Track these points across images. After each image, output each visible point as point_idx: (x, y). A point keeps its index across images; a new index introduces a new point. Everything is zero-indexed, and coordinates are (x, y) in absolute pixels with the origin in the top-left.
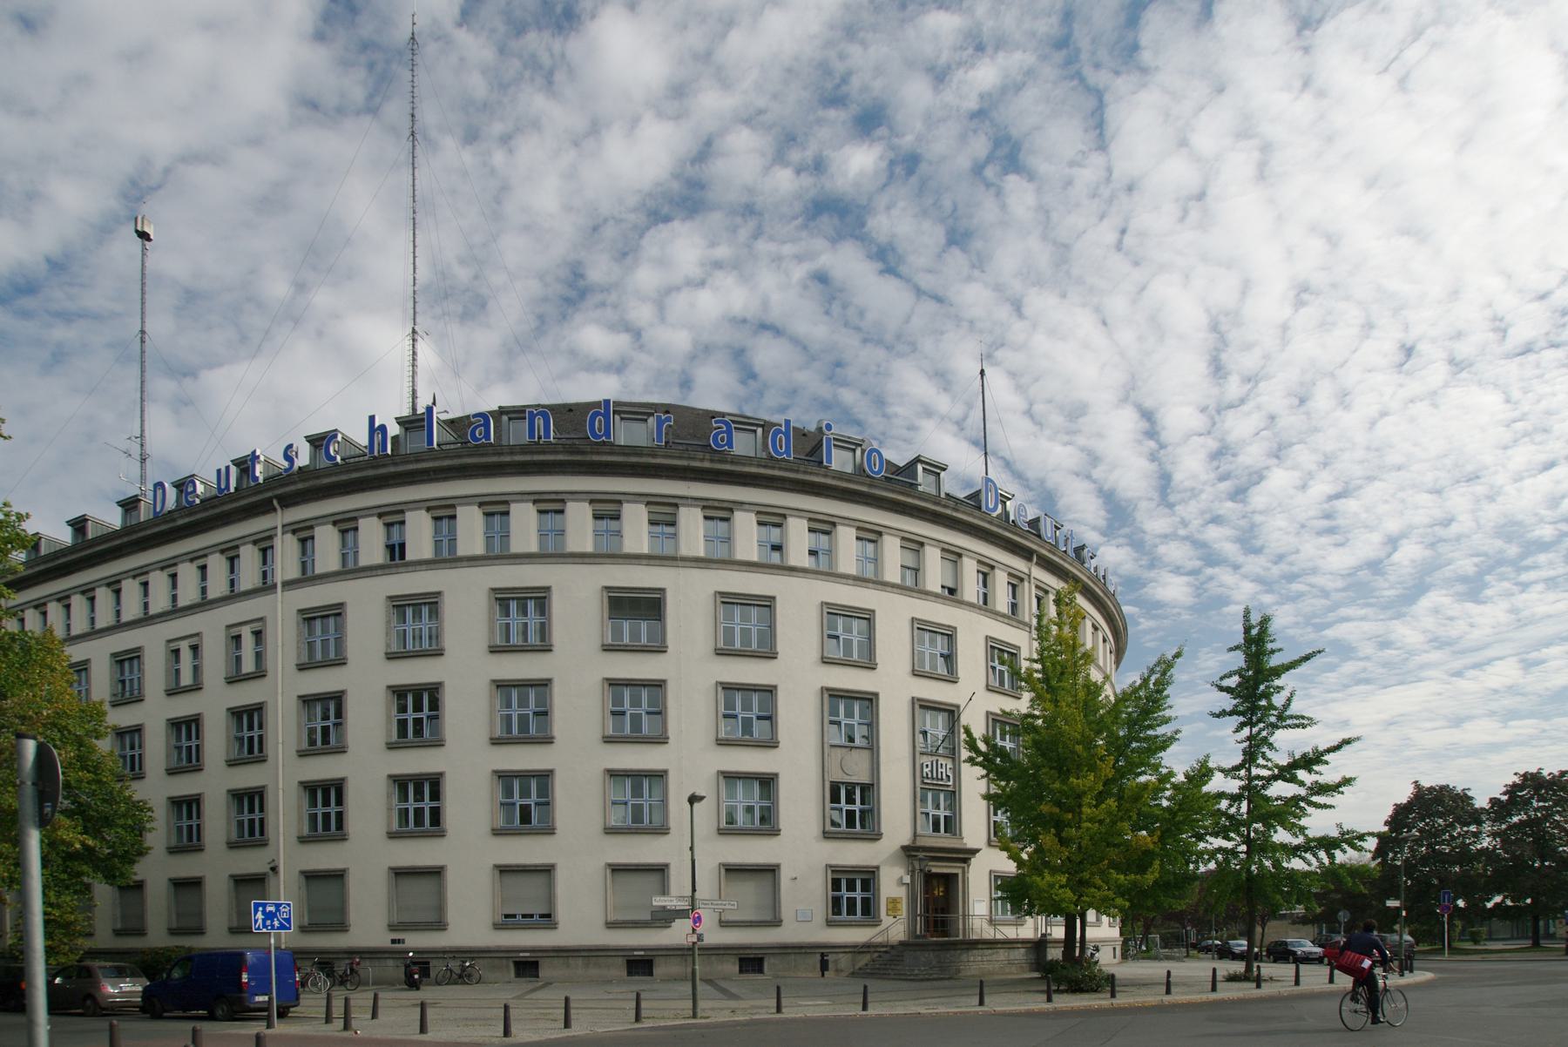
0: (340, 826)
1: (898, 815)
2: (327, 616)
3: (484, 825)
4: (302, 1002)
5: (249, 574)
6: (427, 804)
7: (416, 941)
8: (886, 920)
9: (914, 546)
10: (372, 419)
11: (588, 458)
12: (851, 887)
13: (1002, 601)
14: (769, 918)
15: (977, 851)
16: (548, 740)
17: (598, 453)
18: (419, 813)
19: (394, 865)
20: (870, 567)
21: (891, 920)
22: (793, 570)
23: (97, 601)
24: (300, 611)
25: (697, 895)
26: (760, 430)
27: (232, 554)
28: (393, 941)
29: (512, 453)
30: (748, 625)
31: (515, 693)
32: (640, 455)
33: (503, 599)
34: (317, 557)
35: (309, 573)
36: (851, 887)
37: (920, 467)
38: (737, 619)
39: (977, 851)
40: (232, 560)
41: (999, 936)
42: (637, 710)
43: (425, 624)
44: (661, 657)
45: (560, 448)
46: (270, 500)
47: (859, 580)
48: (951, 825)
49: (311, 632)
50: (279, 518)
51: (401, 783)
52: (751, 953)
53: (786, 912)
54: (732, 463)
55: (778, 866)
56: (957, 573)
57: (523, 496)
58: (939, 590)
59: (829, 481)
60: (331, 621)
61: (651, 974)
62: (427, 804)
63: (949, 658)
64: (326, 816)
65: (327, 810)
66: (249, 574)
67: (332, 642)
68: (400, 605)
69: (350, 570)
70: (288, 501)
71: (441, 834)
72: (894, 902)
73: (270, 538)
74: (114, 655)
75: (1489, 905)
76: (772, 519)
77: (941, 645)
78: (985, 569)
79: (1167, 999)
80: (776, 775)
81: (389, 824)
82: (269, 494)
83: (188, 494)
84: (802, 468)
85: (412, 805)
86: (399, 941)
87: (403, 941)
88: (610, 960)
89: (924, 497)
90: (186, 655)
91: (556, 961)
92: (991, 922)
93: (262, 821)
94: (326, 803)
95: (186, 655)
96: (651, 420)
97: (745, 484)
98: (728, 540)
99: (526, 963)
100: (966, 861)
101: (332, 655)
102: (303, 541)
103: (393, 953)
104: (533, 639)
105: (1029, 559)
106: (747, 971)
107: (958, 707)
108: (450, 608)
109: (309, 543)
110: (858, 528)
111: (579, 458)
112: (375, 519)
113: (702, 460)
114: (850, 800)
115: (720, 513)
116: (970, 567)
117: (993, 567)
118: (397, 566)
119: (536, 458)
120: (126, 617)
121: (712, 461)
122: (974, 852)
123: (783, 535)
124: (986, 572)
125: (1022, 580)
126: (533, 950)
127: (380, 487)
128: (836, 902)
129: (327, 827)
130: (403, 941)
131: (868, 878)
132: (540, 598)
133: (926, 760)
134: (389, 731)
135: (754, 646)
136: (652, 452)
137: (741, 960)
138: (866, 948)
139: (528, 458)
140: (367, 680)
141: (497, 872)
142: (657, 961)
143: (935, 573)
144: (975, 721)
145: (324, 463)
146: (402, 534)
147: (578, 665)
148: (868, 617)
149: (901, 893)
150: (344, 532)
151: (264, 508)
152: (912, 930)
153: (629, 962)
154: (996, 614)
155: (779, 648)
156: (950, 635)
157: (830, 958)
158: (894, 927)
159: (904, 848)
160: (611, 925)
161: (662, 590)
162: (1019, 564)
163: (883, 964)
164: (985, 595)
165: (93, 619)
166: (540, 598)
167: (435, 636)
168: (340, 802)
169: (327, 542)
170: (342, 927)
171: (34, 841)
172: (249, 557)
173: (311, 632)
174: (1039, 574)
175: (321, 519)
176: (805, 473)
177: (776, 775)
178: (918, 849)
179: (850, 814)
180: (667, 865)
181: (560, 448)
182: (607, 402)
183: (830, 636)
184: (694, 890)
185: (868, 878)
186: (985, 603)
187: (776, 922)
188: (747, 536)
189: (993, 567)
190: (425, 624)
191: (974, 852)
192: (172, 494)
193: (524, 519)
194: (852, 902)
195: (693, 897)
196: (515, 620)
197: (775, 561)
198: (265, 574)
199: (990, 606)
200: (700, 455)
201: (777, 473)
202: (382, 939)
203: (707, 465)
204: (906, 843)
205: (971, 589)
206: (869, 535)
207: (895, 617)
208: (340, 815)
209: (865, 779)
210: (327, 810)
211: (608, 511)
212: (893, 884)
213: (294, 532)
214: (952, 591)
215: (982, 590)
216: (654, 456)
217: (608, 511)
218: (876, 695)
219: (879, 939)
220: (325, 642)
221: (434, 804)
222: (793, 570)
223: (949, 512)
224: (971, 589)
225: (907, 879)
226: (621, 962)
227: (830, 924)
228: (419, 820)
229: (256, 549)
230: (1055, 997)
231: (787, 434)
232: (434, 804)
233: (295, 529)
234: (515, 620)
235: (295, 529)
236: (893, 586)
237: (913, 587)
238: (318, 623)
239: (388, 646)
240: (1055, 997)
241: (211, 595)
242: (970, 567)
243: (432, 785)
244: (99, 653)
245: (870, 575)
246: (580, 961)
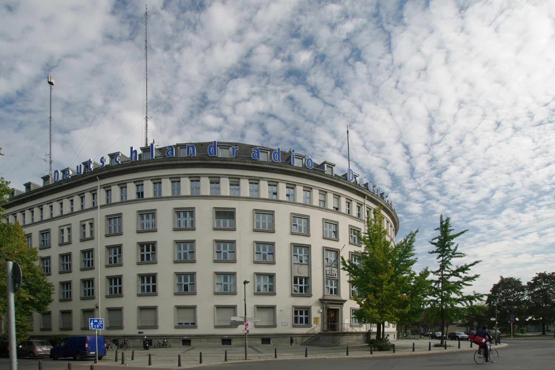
0: (120, 292)
1: (318, 288)
2: (116, 218)
3: (171, 291)
4: (107, 354)
5: (88, 203)
6: (151, 284)
7: (147, 332)
8: (314, 325)
9: (324, 193)
10: (132, 148)
11: (208, 162)
12: (301, 314)
13: (355, 213)
14: (272, 324)
15: (346, 301)
16: (194, 262)
17: (212, 160)
18: (148, 287)
19: (139, 306)
20: (308, 200)
21: (315, 325)
22: (281, 201)
23: (34, 212)
24: (106, 216)
25: (247, 316)
26: (269, 152)
27: (82, 196)
28: (139, 333)
29: (181, 160)
30: (265, 221)
31: (182, 245)
32: (227, 161)
33: (178, 212)
34: (112, 197)
35: (109, 203)
36: (301, 313)
37: (326, 165)
38: (261, 219)
39: (346, 301)
40: (82, 198)
41: (354, 331)
42: (225, 251)
43: (151, 221)
44: (234, 232)
45: (198, 158)
46: (95, 177)
47: (304, 205)
48: (337, 291)
49: (110, 223)
50: (99, 183)
51: (142, 277)
52: (266, 337)
53: (278, 322)
54: (259, 163)
55: (275, 306)
56: (339, 203)
57: (185, 175)
58: (332, 209)
59: (294, 170)
60: (117, 219)
61: (230, 344)
62: (151, 284)
63: (336, 233)
64: (116, 288)
65: (116, 286)
66: (88, 203)
67: (117, 227)
68: (142, 214)
69: (124, 202)
70: (102, 177)
71: (156, 295)
72: (316, 319)
73: (96, 190)
74: (40, 231)
75: (527, 320)
76: (273, 183)
77: (333, 228)
78: (349, 201)
79: (413, 353)
80: (275, 274)
81: (138, 291)
82: (95, 175)
83: (66, 174)
84: (284, 165)
85: (146, 284)
86: (141, 333)
87: (143, 333)
88: (216, 339)
89: (327, 176)
90: (66, 231)
91: (197, 340)
92: (351, 326)
93: (93, 290)
94: (116, 284)
95: (66, 231)
96: (230, 148)
97: (264, 171)
98: (258, 191)
99: (186, 340)
100: (342, 304)
101: (118, 232)
102: (107, 191)
103: (139, 337)
104: (189, 226)
105: (364, 198)
106: (264, 343)
107: (339, 250)
108: (159, 215)
109: (109, 192)
110: (304, 187)
111: (205, 162)
112: (133, 183)
113: (249, 163)
114: (301, 283)
115: (255, 181)
116: (343, 200)
117: (351, 201)
118: (140, 200)
119: (190, 162)
120: (45, 218)
121: (252, 163)
122: (345, 301)
123: (277, 189)
124: (349, 202)
125: (362, 205)
126: (189, 336)
127: (134, 172)
128: (296, 319)
129: (116, 292)
130: (143, 333)
131: (307, 310)
132: (191, 211)
133: (328, 269)
134: (138, 258)
135: (267, 228)
136: (231, 160)
137: (262, 339)
138: (307, 335)
139: (187, 162)
140: (130, 240)
141: (176, 308)
142: (232, 340)
143: (331, 202)
144: (345, 255)
145: (115, 164)
146: (142, 189)
147: (205, 235)
148: (307, 218)
149: (319, 315)
150: (122, 188)
151: (93, 179)
152: (323, 329)
153: (223, 340)
154: (353, 217)
155: (276, 229)
156: (336, 224)
157: (294, 339)
158: (316, 328)
159: (320, 300)
160: (216, 327)
161: (234, 209)
162: (361, 199)
163: (313, 341)
164: (349, 210)
165: (33, 219)
166: (191, 211)
167: (154, 225)
168: (120, 283)
169: (116, 191)
170: (121, 328)
171: (12, 297)
172: (88, 197)
173: (110, 223)
174: (368, 203)
175: (114, 184)
176: (285, 167)
177: (275, 274)
178: (325, 300)
179: (301, 288)
180: (236, 306)
181: (198, 158)
182: (215, 142)
183: (294, 225)
184: (246, 314)
185: (307, 310)
186: (349, 213)
187: (275, 326)
188: (265, 190)
189: (351, 201)
190: (151, 221)
191: (345, 301)
192: (61, 175)
193: (186, 184)
194: (301, 319)
195: (245, 317)
196: (182, 219)
197: (274, 198)
198: (94, 203)
199: (350, 214)
200: (248, 161)
201: (275, 167)
202: (135, 332)
203: (250, 164)
204: (321, 298)
205: (344, 208)
206: (308, 189)
207: (317, 218)
208: (120, 288)
209: (306, 275)
210: (116, 286)
211: (215, 181)
212: (316, 312)
213: (104, 188)
214: (337, 209)
215: (348, 209)
216: (232, 161)
217: (215, 181)
218: (310, 246)
219: (311, 332)
220: (115, 227)
221: (154, 284)
222: (281, 201)
223: (336, 181)
224: (344, 208)
225: (321, 311)
226: (220, 340)
227: (294, 326)
228: (148, 290)
229: (90, 194)
230: (373, 352)
231: (278, 153)
232: (154, 284)
233: (105, 187)
234: (182, 219)
235: (105, 187)
236: (316, 207)
237: (323, 207)
238: (113, 220)
239: (137, 228)
240: (373, 352)
241: (75, 210)
242: (343, 200)
243: (153, 277)
244: (35, 231)
245: (308, 203)
246: (205, 340)
